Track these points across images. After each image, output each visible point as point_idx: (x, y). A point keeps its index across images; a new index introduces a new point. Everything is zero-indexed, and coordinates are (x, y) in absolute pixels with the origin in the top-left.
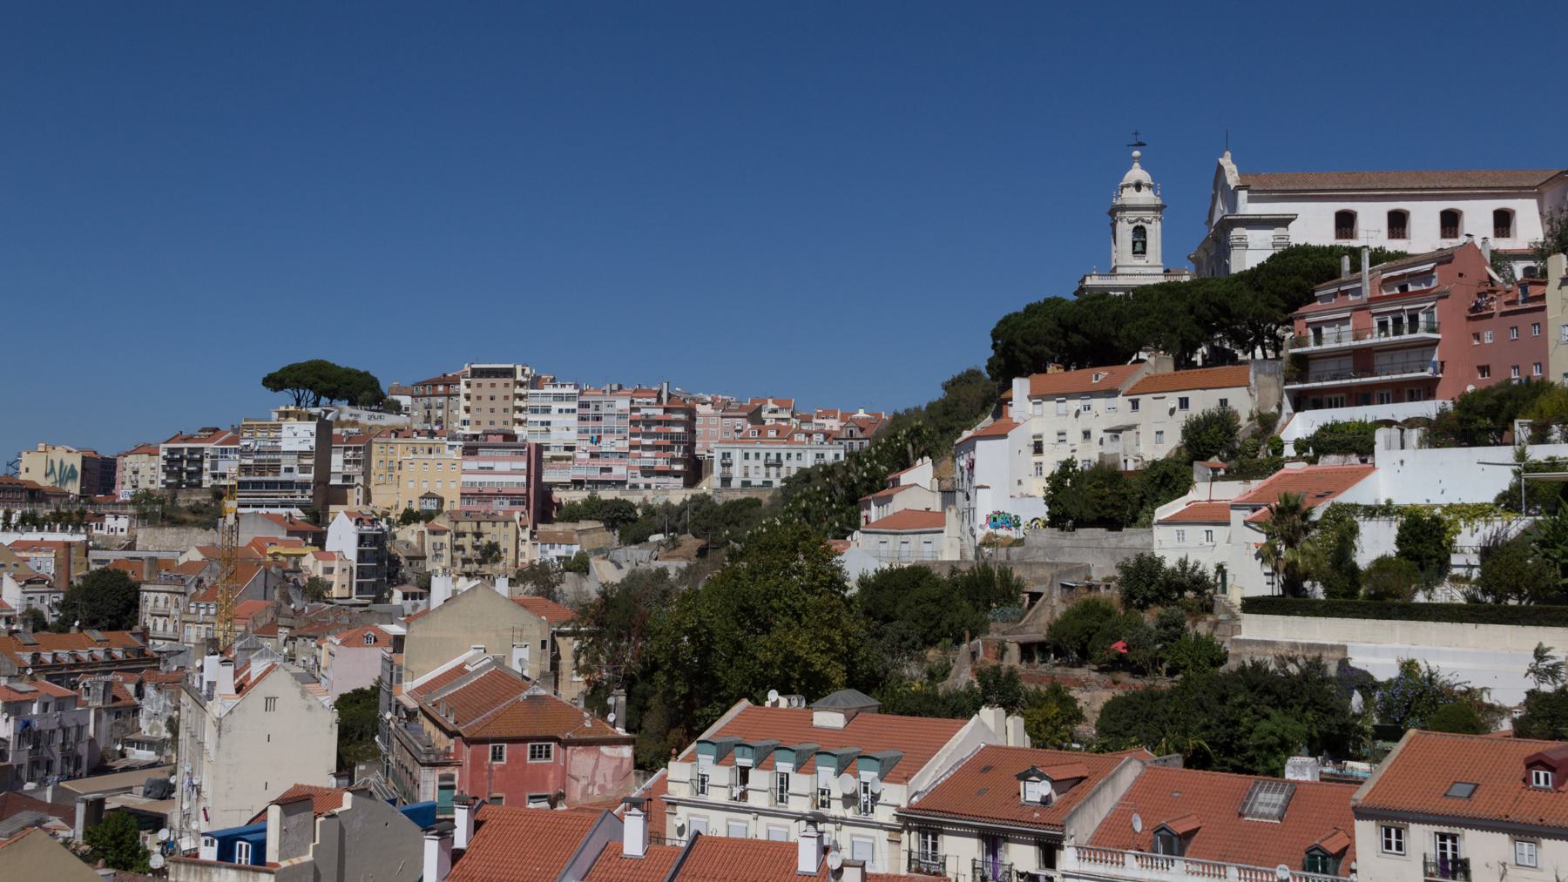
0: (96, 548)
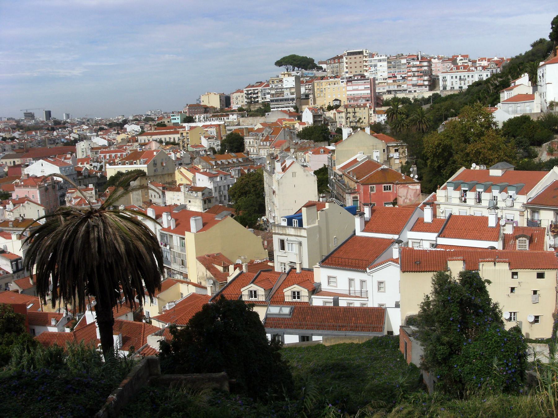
0: (228, 126)
